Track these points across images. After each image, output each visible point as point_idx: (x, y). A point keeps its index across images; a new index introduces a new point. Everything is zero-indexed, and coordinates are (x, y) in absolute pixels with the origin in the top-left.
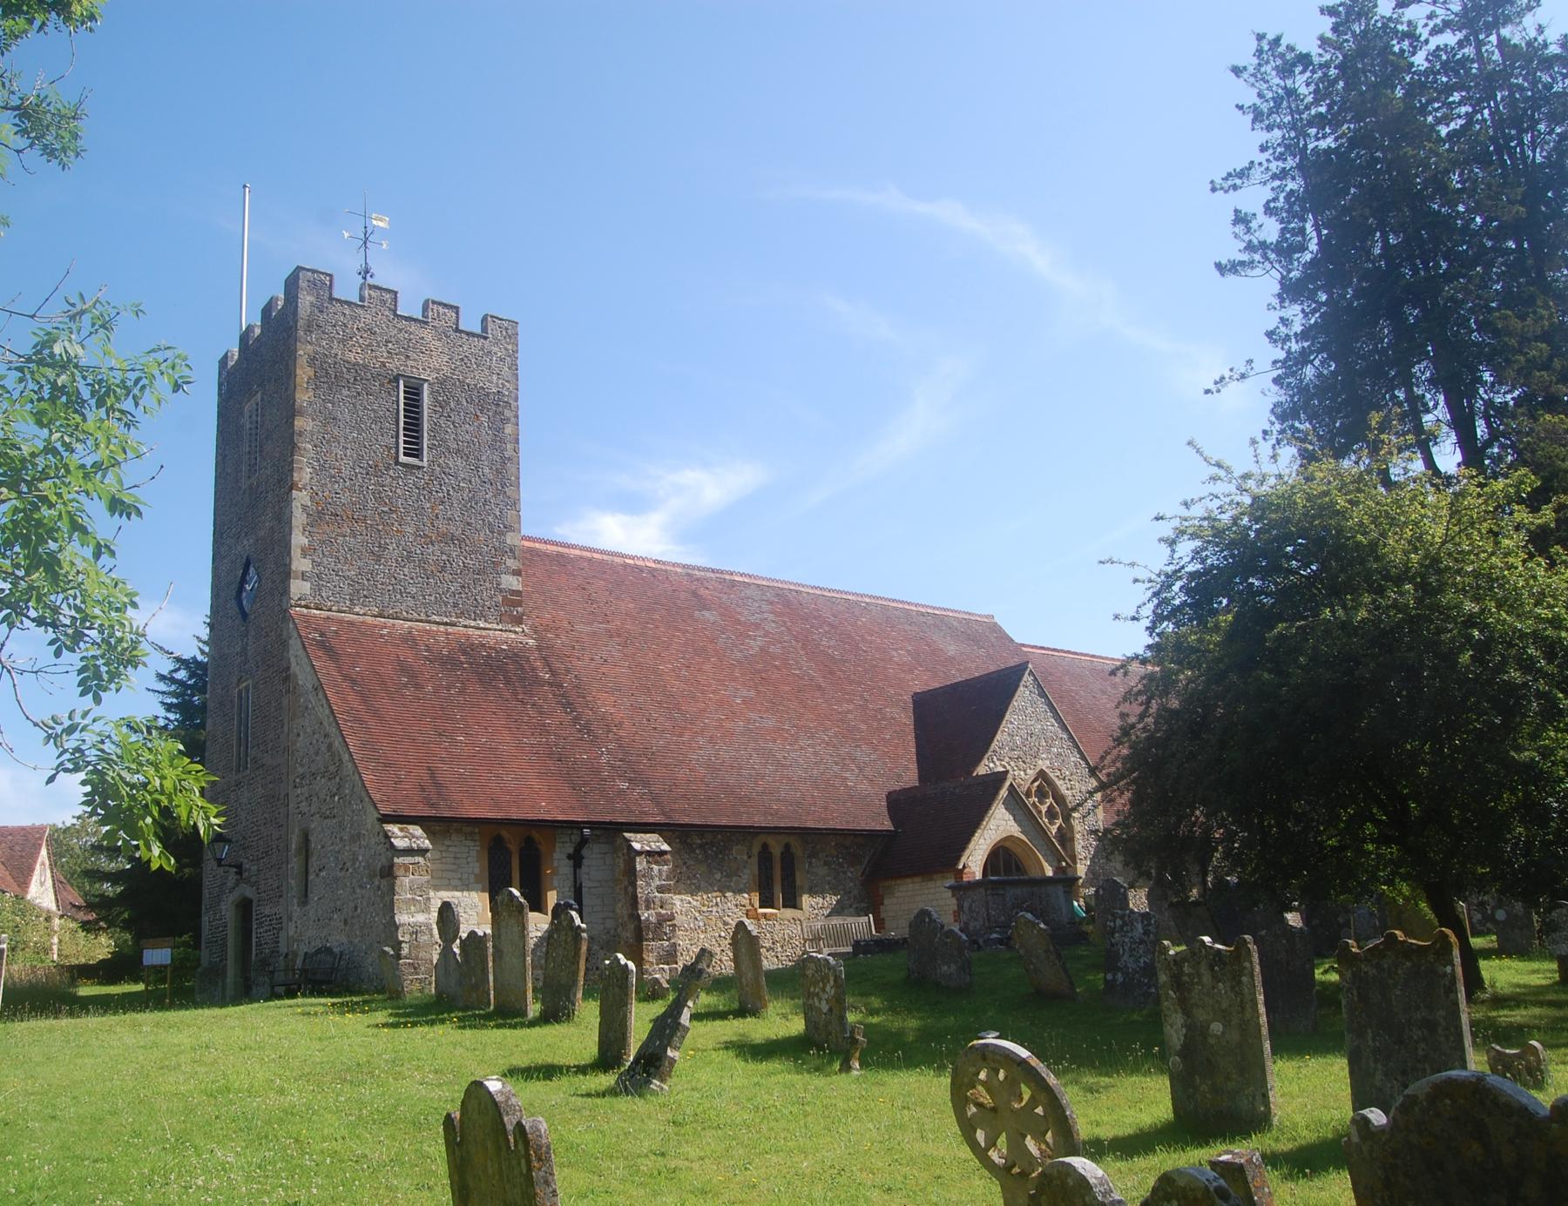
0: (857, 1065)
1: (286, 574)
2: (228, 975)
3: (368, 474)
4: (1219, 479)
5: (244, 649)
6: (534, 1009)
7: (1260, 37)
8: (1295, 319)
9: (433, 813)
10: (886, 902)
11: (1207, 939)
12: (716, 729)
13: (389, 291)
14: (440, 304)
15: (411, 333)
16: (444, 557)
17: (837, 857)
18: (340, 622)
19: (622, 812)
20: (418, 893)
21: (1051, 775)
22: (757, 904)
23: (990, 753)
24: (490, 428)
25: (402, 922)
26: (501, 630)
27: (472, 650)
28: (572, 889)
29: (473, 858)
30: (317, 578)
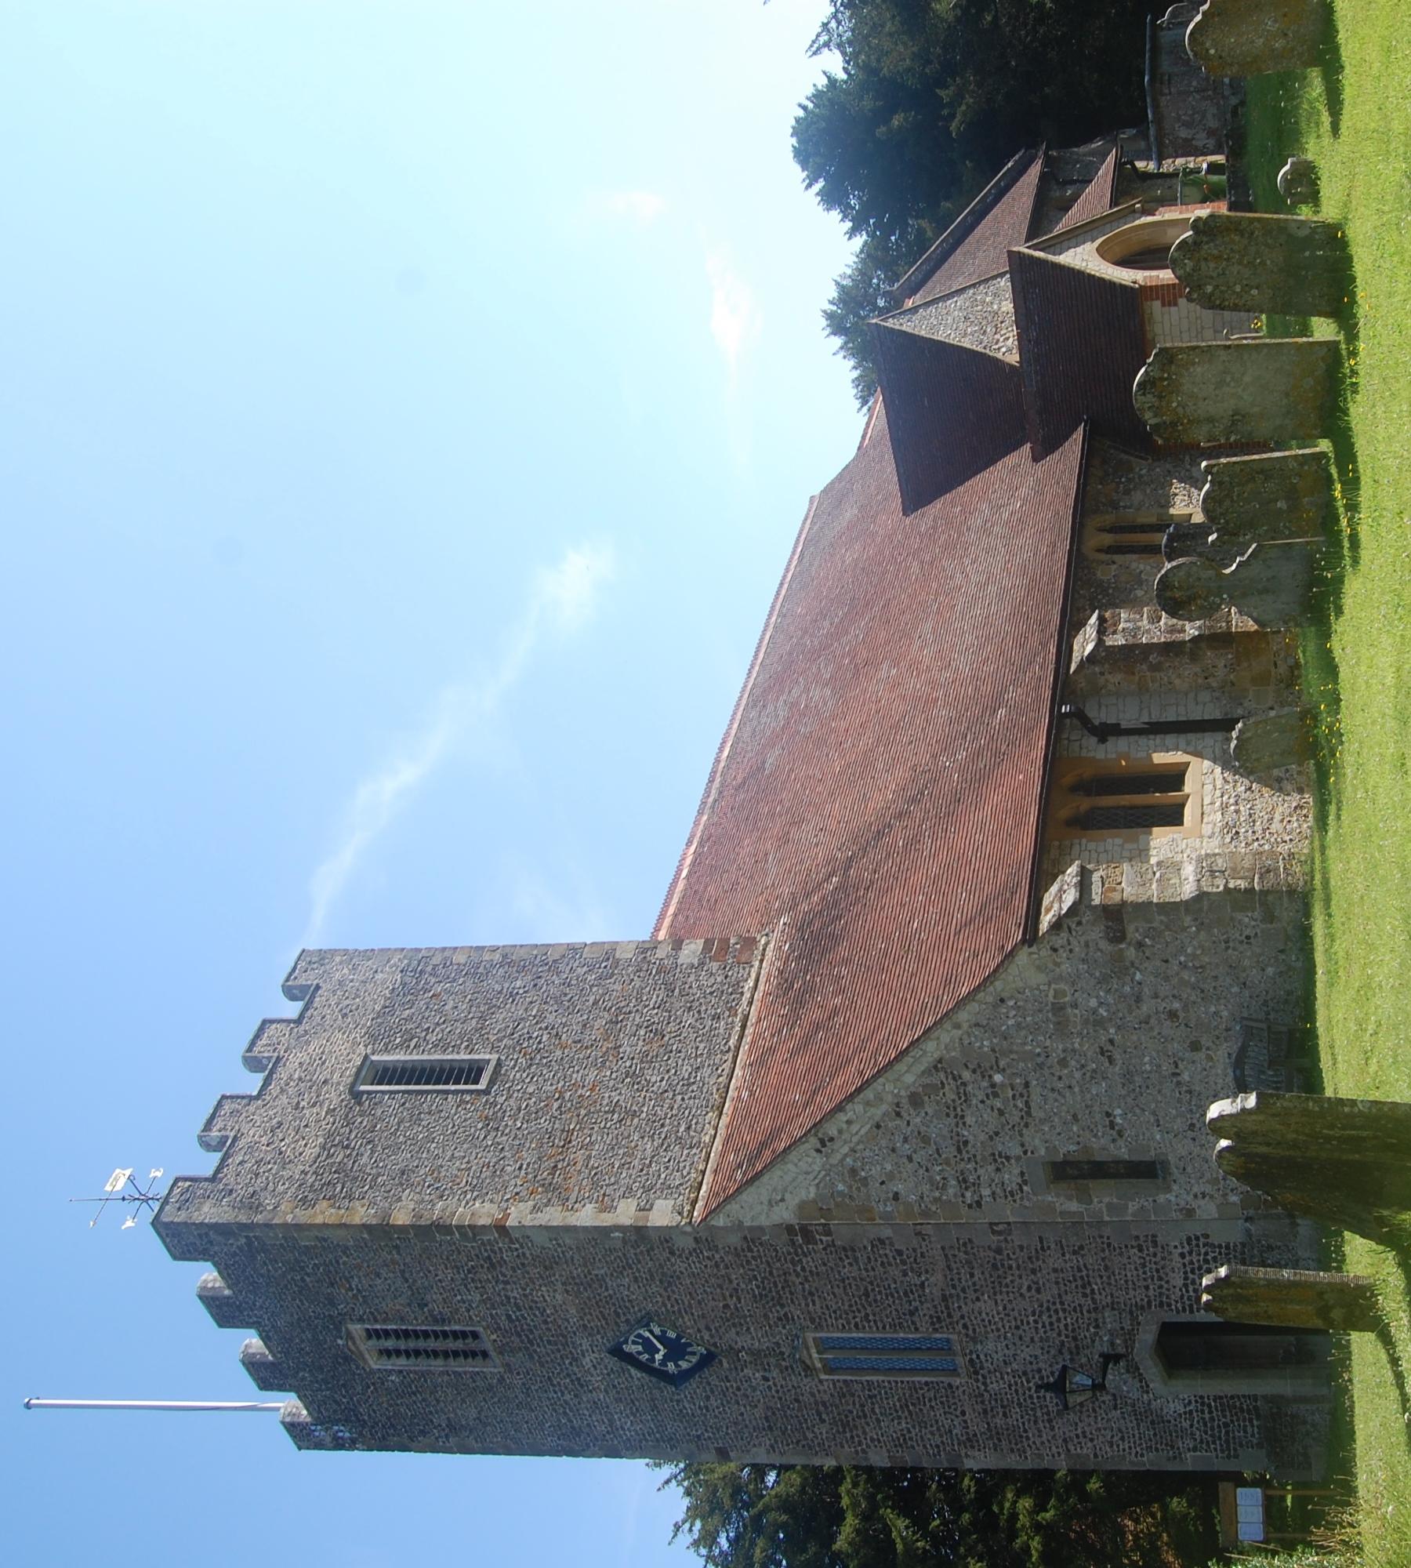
1: (639, 1233)
5: (756, 1354)
6: (1323, 329)
13: (219, 1105)
14: (253, 1043)
15: (291, 1078)
16: (642, 1032)
18: (723, 1154)
20: (1150, 876)
23: (988, 351)
25: (1194, 889)
26: (762, 961)
27: (787, 980)
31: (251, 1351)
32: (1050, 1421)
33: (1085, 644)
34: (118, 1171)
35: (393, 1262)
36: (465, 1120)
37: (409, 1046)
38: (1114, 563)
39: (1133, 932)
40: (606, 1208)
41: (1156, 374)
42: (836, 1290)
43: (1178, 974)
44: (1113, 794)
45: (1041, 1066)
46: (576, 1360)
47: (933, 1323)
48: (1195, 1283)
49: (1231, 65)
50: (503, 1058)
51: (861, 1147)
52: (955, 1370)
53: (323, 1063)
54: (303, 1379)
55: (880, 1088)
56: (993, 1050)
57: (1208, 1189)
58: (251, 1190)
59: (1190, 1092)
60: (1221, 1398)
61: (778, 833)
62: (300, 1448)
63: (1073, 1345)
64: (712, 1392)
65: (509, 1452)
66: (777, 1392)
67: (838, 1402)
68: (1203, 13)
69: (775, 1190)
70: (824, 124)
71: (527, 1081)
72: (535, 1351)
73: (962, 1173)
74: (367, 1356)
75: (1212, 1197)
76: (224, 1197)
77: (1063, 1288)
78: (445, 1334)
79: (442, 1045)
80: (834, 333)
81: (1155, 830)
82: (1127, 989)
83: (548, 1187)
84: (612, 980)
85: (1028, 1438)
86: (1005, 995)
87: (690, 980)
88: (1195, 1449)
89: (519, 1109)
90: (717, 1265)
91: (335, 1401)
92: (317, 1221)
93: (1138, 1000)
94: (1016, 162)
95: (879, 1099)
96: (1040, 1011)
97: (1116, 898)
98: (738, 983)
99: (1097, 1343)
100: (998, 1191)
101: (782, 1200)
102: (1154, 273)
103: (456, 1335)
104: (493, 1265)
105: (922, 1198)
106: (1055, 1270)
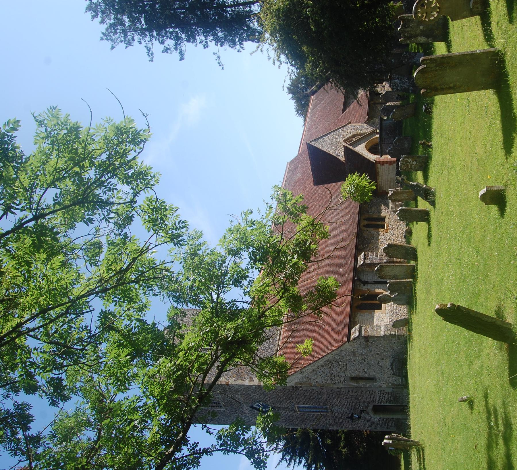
0: (430, 143)
2: (398, 417)
4: (262, 49)
5: (284, 409)
6: (413, 263)
7: (102, 39)
8: (200, 39)
9: (347, 326)
10: (385, 190)
11: (399, 28)
12: (323, 245)
19: (350, 269)
21: (345, 138)
22: (383, 229)
29: (362, 315)
40: (251, 380)
44: (367, 300)
45: (350, 361)
57: (385, 382)
80: (289, 93)
81: (376, 311)
93: (371, 351)
97: (367, 334)
103: (214, 403)
104: (225, 391)
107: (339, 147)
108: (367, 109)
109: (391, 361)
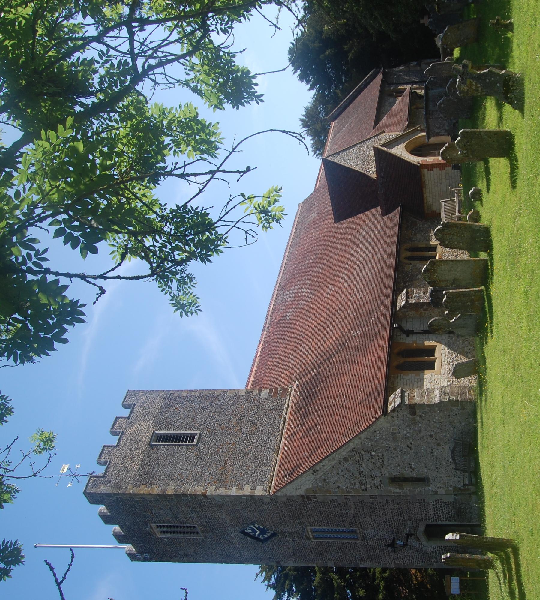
1: (252, 498)
3: (201, 459)
5: (291, 534)
6: (483, 256)
10: (435, 209)
14: (113, 426)
15: (128, 439)
17: (413, 230)
18: (279, 470)
20: (424, 394)
23: (365, 172)
24: (183, 403)
25: (439, 399)
26: (290, 397)
27: (299, 407)
28: (424, 335)
30: (255, 483)
31: (116, 531)
32: (389, 553)
33: (401, 301)
34: (64, 465)
35: (167, 505)
36: (190, 456)
37: (168, 428)
38: (411, 264)
39: (419, 412)
41: (430, 268)
42: (318, 515)
43: (433, 424)
44: (413, 357)
45: (388, 450)
46: (229, 535)
47: (350, 524)
48: (441, 557)
49: (455, 161)
50: (202, 432)
51: (327, 473)
52: (357, 538)
53: (139, 433)
54: (134, 540)
55: (334, 456)
56: (372, 445)
57: (442, 486)
58: (117, 481)
59: (437, 458)
60: (446, 547)
61: (293, 346)
62: (132, 561)
63: (397, 531)
64: (275, 544)
65: (205, 562)
66: (297, 544)
67: (317, 547)
68: (446, 147)
69: (298, 485)
70: (300, 51)
71: (211, 441)
72: (215, 532)
73: (361, 480)
74: (157, 533)
75: (443, 488)
76: (108, 483)
77: (394, 514)
78: (184, 527)
79: (180, 428)
81: (426, 371)
82: (417, 428)
83: (220, 481)
84: (238, 404)
85: (381, 558)
86: (376, 430)
87: (265, 404)
88: (437, 562)
89: (208, 452)
90: (278, 507)
91: (145, 547)
92: (141, 493)
93: (420, 431)
94: (372, 73)
95: (334, 459)
96: (388, 434)
97: (413, 402)
98: (282, 406)
99: (405, 531)
100: (373, 486)
101: (301, 488)
102: (425, 158)
103: (187, 527)
104: (201, 506)
105: (347, 488)
106: (391, 509)
107: (368, 162)
108: (407, 115)
109: (452, 448)
